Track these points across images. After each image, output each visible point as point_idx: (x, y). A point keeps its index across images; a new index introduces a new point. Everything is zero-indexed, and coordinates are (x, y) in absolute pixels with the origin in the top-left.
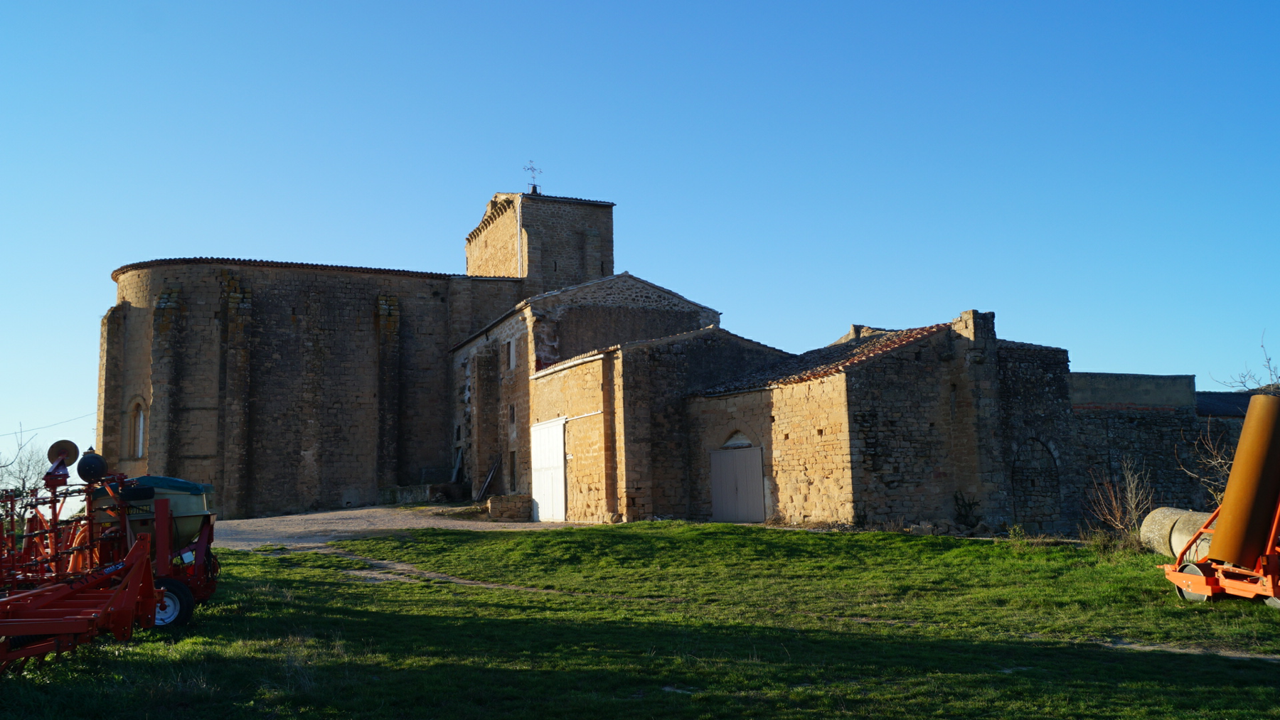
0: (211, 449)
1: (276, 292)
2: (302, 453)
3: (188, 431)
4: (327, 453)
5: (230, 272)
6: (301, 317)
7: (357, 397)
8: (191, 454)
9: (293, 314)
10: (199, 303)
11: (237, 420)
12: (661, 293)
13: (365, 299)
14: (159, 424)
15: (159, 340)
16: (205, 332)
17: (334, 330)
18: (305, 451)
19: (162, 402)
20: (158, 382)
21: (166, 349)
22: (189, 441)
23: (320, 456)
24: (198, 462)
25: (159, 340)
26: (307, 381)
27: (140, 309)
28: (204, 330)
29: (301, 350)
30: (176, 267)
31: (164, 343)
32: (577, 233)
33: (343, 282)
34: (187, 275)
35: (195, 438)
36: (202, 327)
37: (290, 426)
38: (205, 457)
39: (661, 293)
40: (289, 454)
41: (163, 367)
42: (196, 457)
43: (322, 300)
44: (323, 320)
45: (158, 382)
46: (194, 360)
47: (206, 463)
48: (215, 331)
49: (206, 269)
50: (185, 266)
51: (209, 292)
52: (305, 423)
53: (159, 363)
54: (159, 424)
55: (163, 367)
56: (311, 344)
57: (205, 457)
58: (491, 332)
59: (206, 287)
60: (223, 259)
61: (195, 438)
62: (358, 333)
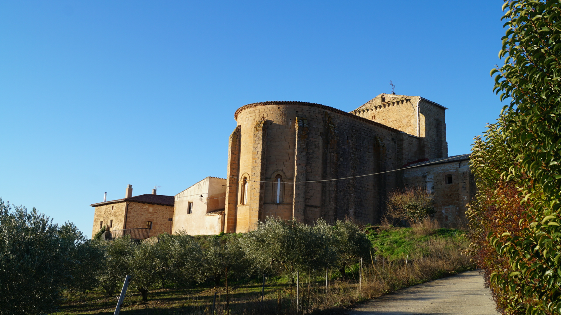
0: (318, 203)
1: (342, 127)
2: (349, 210)
3: (308, 192)
4: (357, 212)
5: (326, 114)
6: (350, 141)
7: (367, 185)
8: (310, 204)
9: (347, 139)
10: (314, 127)
11: (334, 189)
12: (239, 138)
13: (370, 137)
14: (301, 186)
15: (301, 143)
16: (316, 142)
17: (361, 150)
18: (350, 209)
19: (302, 175)
20: (300, 164)
21: (304, 148)
22: (309, 197)
23: (355, 213)
24: (313, 209)
25: (301, 143)
26: (351, 174)
27: (280, 125)
28: (316, 141)
29: (350, 158)
30: (303, 107)
31: (303, 145)
32: (435, 120)
33: (364, 127)
34: (308, 111)
35: (311, 196)
36: (315, 139)
37: (345, 196)
38: (316, 207)
39: (239, 138)
40: (345, 210)
41: (303, 157)
42: (312, 206)
43: (357, 134)
44: (357, 144)
45: (300, 164)
46: (311, 156)
47: (316, 210)
48: (320, 142)
49: (317, 110)
50: (307, 107)
51: (318, 122)
52: (350, 196)
53: (300, 155)
54: (301, 186)
55: (303, 157)
56: (353, 155)
57: (316, 207)
58: (463, 162)
59: (317, 119)
60: (299, 102)
61: (311, 196)
62: (368, 153)
